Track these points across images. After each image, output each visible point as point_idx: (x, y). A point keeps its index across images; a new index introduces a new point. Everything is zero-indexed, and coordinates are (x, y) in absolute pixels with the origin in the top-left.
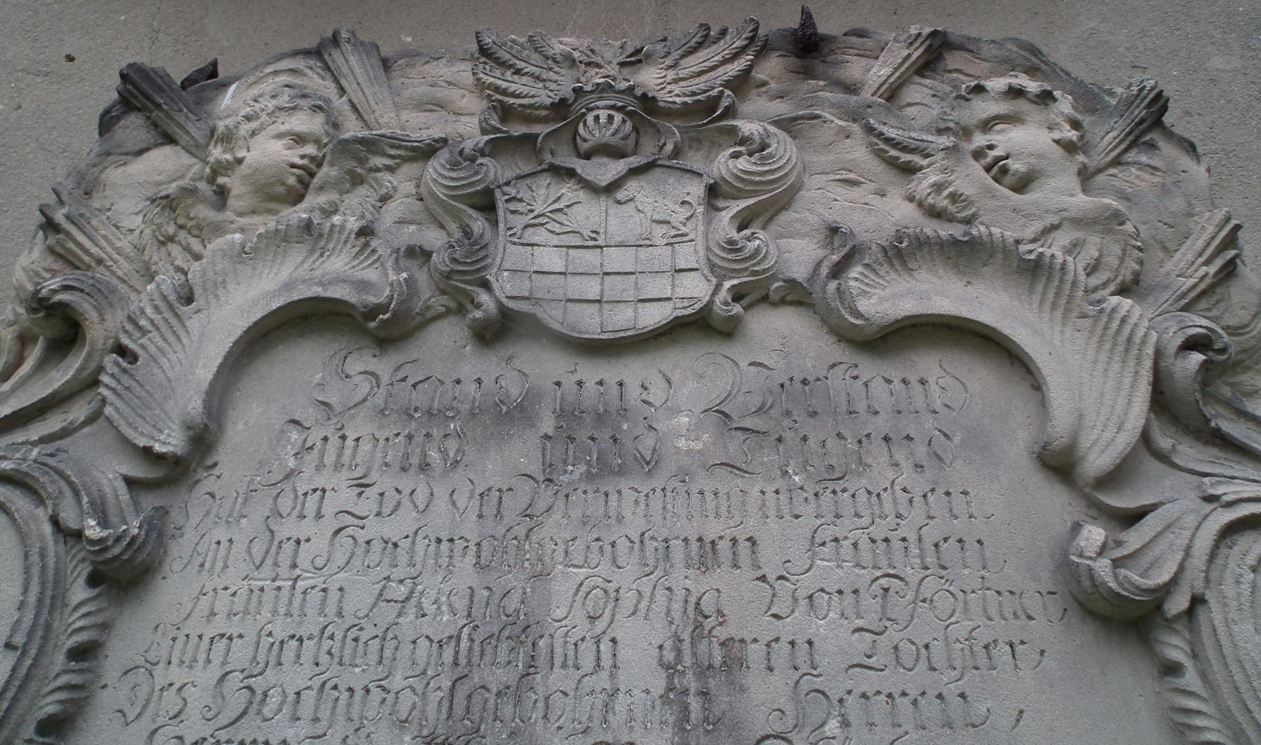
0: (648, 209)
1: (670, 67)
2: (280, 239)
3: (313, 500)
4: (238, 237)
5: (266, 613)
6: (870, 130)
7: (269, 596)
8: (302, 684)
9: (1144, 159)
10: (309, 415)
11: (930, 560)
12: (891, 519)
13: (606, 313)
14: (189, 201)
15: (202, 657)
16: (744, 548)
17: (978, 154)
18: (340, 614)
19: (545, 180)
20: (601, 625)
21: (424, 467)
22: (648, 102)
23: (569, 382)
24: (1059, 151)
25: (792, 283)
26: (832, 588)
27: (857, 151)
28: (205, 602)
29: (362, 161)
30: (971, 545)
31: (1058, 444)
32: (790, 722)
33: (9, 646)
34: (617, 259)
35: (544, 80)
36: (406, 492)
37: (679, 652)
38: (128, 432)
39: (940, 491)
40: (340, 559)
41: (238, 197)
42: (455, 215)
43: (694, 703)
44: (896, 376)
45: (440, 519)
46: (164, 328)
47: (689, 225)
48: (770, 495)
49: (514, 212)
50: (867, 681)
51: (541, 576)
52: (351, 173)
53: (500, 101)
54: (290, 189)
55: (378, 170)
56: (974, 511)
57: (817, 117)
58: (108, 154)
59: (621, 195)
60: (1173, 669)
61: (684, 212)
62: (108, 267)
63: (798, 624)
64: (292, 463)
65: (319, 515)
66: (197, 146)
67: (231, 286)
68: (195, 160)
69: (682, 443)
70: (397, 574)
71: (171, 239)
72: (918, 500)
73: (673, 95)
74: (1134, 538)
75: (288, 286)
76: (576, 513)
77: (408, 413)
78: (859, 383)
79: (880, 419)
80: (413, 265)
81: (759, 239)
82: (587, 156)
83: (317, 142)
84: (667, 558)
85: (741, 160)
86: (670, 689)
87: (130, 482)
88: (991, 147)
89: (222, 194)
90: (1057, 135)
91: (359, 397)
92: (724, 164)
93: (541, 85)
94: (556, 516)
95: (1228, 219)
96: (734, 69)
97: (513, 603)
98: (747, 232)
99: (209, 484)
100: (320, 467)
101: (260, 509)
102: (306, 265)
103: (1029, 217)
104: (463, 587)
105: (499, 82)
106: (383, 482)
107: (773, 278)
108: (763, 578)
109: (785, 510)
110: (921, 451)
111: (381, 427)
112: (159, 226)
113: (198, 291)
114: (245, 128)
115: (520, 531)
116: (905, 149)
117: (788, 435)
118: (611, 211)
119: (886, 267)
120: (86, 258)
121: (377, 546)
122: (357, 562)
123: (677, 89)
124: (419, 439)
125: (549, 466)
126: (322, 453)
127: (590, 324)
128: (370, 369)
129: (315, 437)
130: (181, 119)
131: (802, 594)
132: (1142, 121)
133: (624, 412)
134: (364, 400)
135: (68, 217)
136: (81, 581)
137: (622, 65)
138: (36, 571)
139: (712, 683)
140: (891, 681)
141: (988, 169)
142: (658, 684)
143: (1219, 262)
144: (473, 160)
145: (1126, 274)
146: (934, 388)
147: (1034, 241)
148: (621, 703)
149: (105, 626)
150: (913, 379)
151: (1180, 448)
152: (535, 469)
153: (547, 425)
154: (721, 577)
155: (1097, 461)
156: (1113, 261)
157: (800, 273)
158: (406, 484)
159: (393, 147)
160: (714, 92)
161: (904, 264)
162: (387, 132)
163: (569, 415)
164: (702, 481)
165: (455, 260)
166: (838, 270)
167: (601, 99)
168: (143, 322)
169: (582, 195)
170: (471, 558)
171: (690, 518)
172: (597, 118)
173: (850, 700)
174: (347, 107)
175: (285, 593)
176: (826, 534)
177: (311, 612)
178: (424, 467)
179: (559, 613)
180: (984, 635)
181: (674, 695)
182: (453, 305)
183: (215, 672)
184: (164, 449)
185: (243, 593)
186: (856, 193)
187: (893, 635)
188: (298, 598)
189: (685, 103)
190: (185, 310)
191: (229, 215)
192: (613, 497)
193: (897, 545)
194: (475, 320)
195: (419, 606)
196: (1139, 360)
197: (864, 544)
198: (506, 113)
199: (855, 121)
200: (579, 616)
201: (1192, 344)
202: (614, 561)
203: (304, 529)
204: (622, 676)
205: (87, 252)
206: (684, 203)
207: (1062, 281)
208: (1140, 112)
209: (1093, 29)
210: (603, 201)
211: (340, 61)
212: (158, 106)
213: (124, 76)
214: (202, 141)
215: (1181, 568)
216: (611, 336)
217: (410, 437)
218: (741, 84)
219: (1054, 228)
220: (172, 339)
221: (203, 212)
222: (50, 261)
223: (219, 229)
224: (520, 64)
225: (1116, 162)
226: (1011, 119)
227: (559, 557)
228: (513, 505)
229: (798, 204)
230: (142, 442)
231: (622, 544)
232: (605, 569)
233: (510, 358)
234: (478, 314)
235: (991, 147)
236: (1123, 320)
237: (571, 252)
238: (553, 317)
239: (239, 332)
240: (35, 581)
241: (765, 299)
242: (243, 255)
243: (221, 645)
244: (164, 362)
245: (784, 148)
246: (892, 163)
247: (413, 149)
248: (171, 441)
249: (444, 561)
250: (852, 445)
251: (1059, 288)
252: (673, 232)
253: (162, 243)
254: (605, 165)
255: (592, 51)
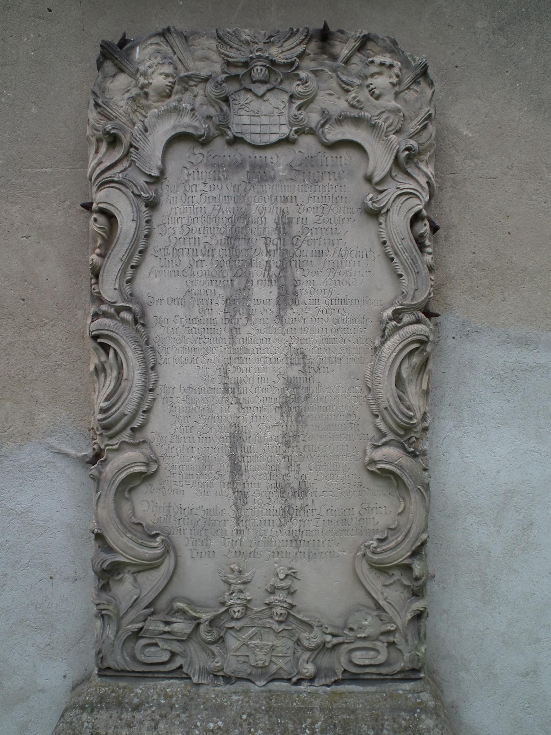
0: (273, 104)
1: (280, 47)
2: (170, 112)
3: (194, 187)
4: (156, 110)
5: (189, 213)
6: (338, 76)
7: (188, 209)
8: (200, 227)
9: (415, 88)
10: (188, 165)
11: (334, 201)
12: (327, 192)
13: (262, 137)
14: (139, 98)
15: (176, 222)
16: (294, 198)
17: (368, 86)
18: (205, 213)
19: (243, 92)
20: (262, 215)
21: (219, 179)
22: (273, 63)
23: (253, 156)
24: (390, 86)
25: (311, 129)
26: (312, 207)
27: (334, 83)
28: (173, 211)
29: (187, 83)
30: (344, 198)
31: (368, 174)
32: (301, 233)
33: (133, 220)
34: (264, 120)
35: (240, 50)
36: (216, 185)
37: (279, 220)
38: (143, 170)
39: (339, 186)
40: (203, 201)
41: (152, 96)
42: (218, 103)
43: (282, 230)
44: (334, 155)
45: (225, 192)
46: (143, 140)
47: (284, 109)
48: (300, 186)
49: (235, 104)
50: (317, 226)
51: (249, 204)
52: (184, 88)
53: (227, 60)
54: (167, 93)
55: (192, 86)
56: (346, 190)
57: (323, 70)
58: (105, 77)
59: (265, 98)
60: (381, 224)
61: (282, 105)
62: (119, 120)
63: (304, 214)
64: (186, 178)
65: (196, 191)
66: (133, 74)
67: (158, 127)
68: (132, 79)
69: (281, 174)
70: (216, 204)
71: (136, 110)
72: (334, 188)
73: (281, 59)
74: (380, 197)
75: (174, 127)
76: (256, 190)
77: (213, 165)
78: (325, 158)
79: (328, 168)
80: (208, 121)
81: (302, 115)
82: (254, 82)
83: (173, 76)
84: (277, 200)
85: (300, 87)
86: (277, 227)
87: (146, 182)
88: (372, 84)
89: (146, 94)
90: (391, 80)
91: (200, 161)
92: (295, 88)
93: (239, 52)
94: (251, 191)
95: (428, 112)
96: (300, 49)
97: (243, 210)
98: (300, 112)
99: (166, 183)
100: (194, 179)
101: (182, 190)
102: (178, 120)
103: (377, 108)
104: (232, 207)
105: (226, 52)
106: (210, 183)
107: (306, 127)
108: (297, 205)
109: (304, 190)
110: (337, 175)
111: (207, 169)
112: (132, 107)
113: (149, 128)
114: (150, 71)
115: (244, 195)
116: (347, 84)
117: (306, 172)
118: (263, 104)
119: (336, 125)
120: (112, 117)
121: (211, 198)
122: (207, 202)
123: (282, 56)
124: (217, 172)
125: (249, 179)
126: (194, 175)
127: (257, 140)
128: (202, 152)
129: (191, 171)
130: (125, 64)
131: (305, 208)
132: (418, 75)
133: (267, 165)
134: (201, 161)
135: (103, 102)
136: (143, 206)
137: (265, 43)
138: (133, 204)
139: (285, 226)
140: (322, 226)
141: (370, 91)
142: (274, 226)
143: (422, 125)
144: (221, 85)
145: (398, 128)
146: (343, 159)
147: (377, 116)
148: (267, 230)
149: (151, 216)
150: (338, 157)
151: (398, 175)
152: (246, 180)
153: (248, 169)
154: (288, 205)
155: (376, 179)
156: (395, 123)
157: (313, 125)
158: (216, 183)
159: (196, 78)
160: (293, 60)
161: (341, 124)
162: (193, 72)
163: (253, 166)
164: (286, 183)
165: (220, 121)
166: (323, 126)
167: (258, 61)
168: (138, 139)
169: (254, 98)
170: (233, 201)
171: (282, 191)
172: (257, 70)
173: (313, 229)
174: (177, 60)
175: (192, 208)
176: (312, 195)
177: (199, 212)
178: (219, 179)
179: (253, 212)
180: (342, 217)
181: (278, 228)
182: (220, 133)
183: (180, 225)
184: (155, 175)
185: (182, 208)
186: (332, 98)
187: (324, 217)
188: (195, 210)
189: (284, 62)
190: (147, 134)
191: (150, 102)
192: (264, 187)
193: (327, 198)
194: (227, 139)
195: (223, 211)
196: (392, 154)
197: (320, 198)
198: (228, 64)
199: (334, 72)
200: (257, 213)
201: (407, 149)
202: (265, 201)
203: (194, 194)
204: (267, 225)
205: (112, 114)
206: (283, 102)
207: (380, 130)
208: (418, 71)
209: (440, 5)
210: (260, 101)
211: (173, 40)
212: (117, 59)
213: (101, 46)
214: (134, 73)
215: (387, 203)
216: (263, 144)
217: (215, 172)
218: (301, 56)
219: (383, 112)
220: (145, 143)
221: (143, 101)
222: (100, 116)
223: (149, 107)
224: (232, 44)
225: (408, 88)
226: (380, 74)
227: (253, 200)
228: (241, 188)
229: (316, 102)
230: (148, 173)
231: (267, 197)
232: (263, 203)
233: (237, 150)
234: (228, 138)
235: (372, 84)
236: (391, 143)
237: (252, 117)
238: (247, 138)
239: (165, 142)
240: (134, 206)
241: (304, 132)
242: (160, 117)
243: (180, 219)
244: (145, 150)
245: (313, 83)
246: (343, 88)
247: (202, 79)
248: (156, 173)
249: (227, 201)
250: (320, 174)
251: (379, 132)
252: (280, 112)
253: (134, 112)
254: (260, 87)
255: (255, 37)
